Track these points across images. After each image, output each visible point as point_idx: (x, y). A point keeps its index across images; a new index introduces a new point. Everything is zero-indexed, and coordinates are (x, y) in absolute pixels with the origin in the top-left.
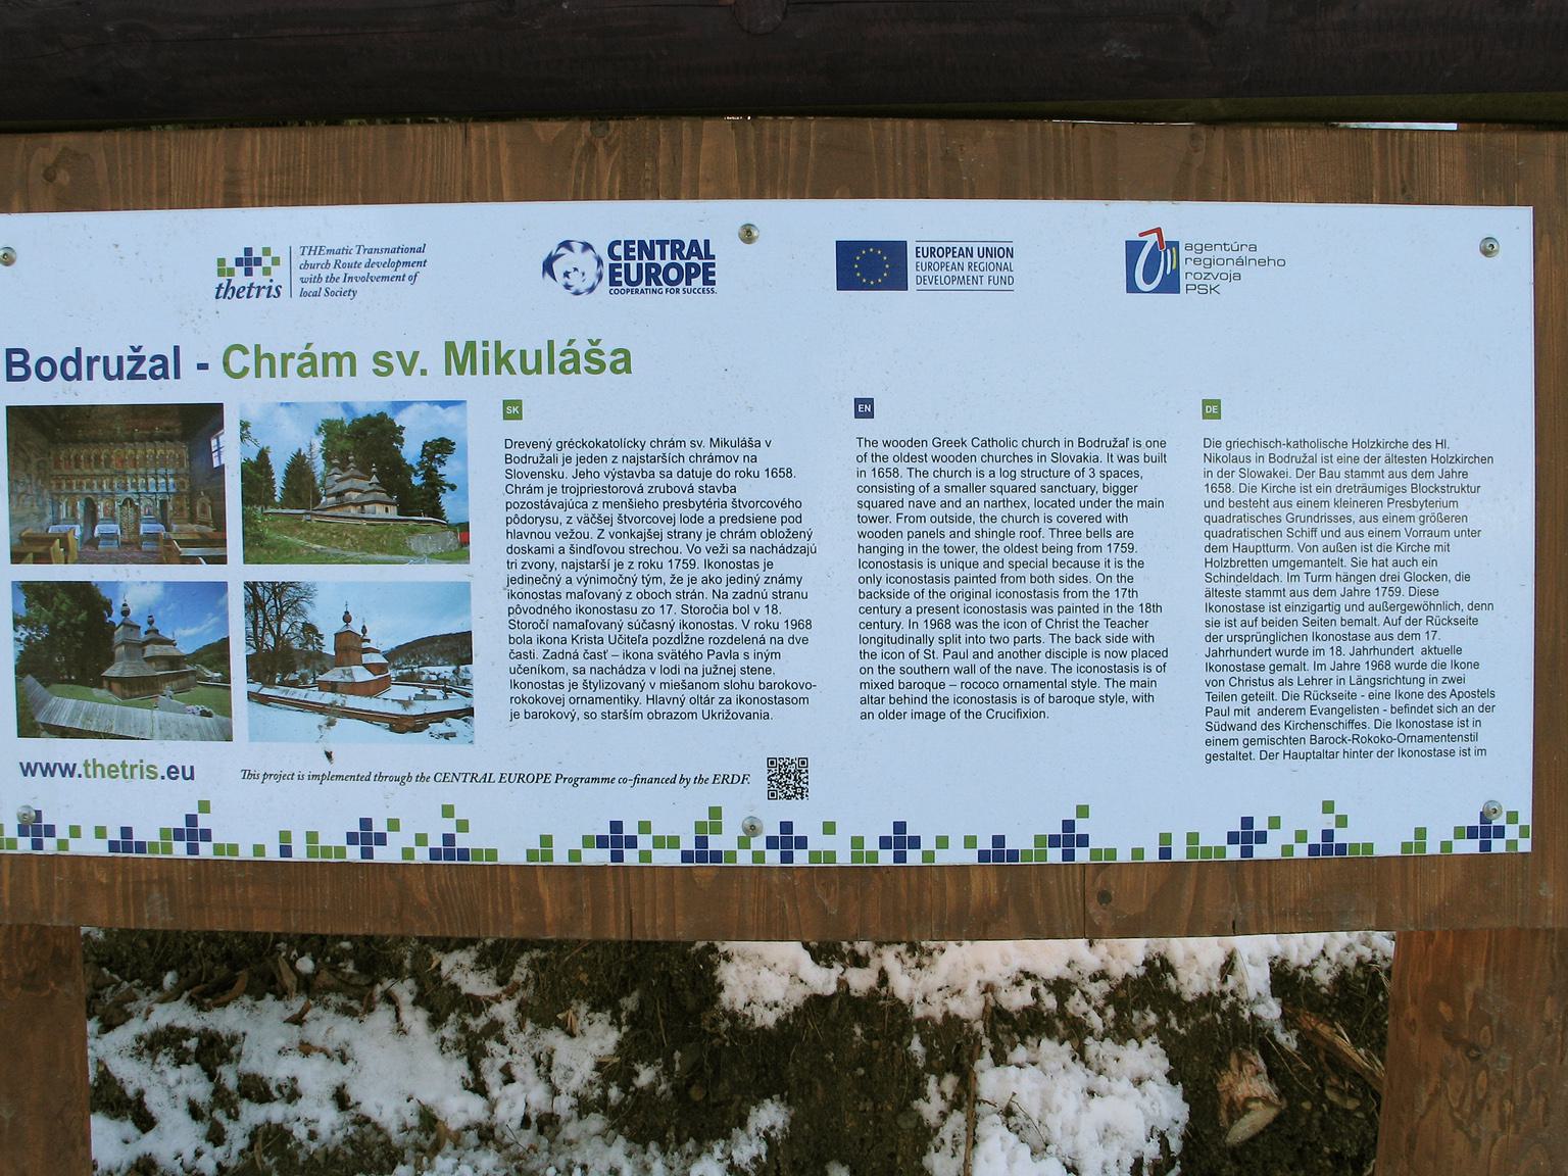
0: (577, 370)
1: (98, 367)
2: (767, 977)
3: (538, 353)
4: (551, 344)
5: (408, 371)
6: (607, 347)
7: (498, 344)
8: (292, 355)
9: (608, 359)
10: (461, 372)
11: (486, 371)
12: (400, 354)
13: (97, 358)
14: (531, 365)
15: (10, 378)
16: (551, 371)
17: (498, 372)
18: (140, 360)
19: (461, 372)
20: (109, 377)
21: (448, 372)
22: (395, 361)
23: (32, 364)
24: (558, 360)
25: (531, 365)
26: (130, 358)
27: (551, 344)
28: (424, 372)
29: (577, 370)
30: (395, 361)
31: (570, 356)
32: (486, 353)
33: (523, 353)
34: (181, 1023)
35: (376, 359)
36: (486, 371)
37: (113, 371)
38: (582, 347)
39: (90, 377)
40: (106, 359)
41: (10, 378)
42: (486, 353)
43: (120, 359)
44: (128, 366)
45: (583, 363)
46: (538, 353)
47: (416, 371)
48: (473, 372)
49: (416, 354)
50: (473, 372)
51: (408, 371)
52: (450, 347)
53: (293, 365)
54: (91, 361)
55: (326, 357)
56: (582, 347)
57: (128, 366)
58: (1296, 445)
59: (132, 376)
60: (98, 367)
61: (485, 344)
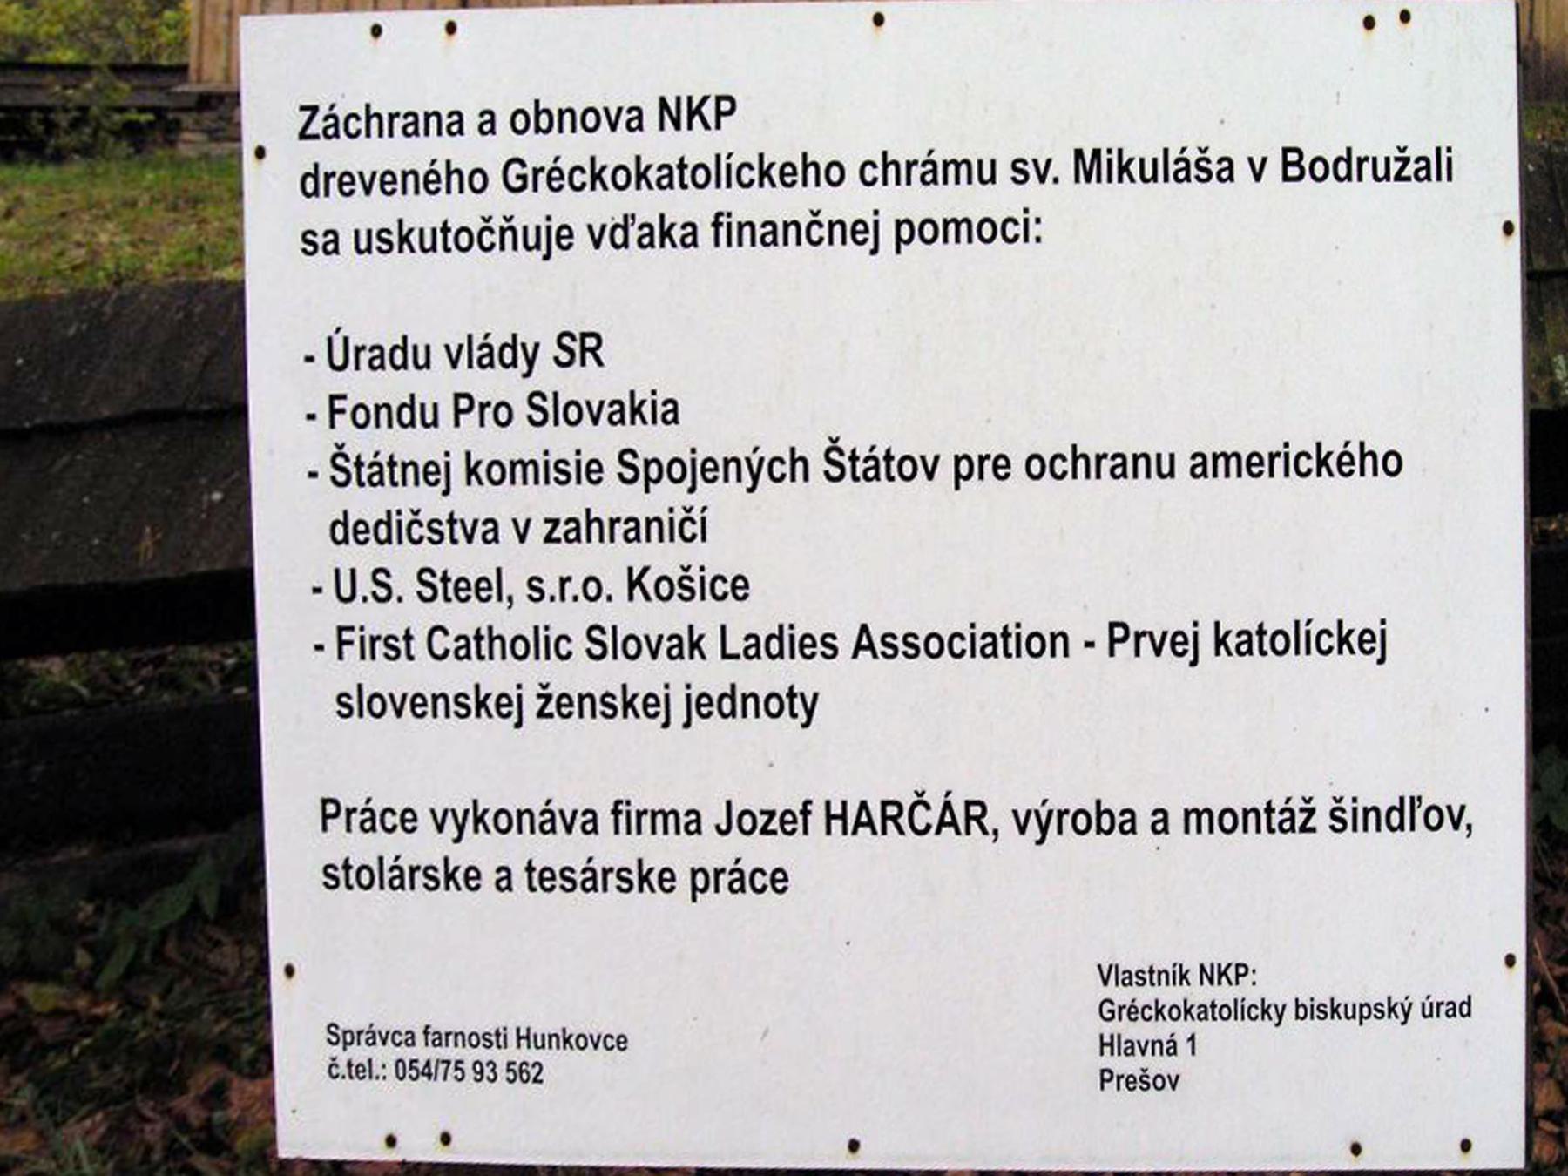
0: (1188, 178)
1: (1367, 167)
2: (171, 116)
3: (1155, 161)
4: (1166, 151)
5: (1042, 179)
6: (1213, 155)
7: (1120, 151)
8: (915, 162)
9: (1214, 168)
10: (1088, 180)
11: (1110, 180)
12: (1035, 162)
13: (1366, 159)
14: (1149, 174)
15: (1286, 178)
16: (1166, 180)
17: (1120, 180)
18: (1406, 161)
19: (1088, 180)
20: (1377, 179)
21: (1077, 180)
22: (1030, 169)
23: (1306, 163)
24: (1172, 168)
25: (1149, 174)
26: (1397, 159)
27: (1166, 151)
28: (1056, 180)
29: (1188, 178)
30: (1030, 169)
31: (1182, 165)
32: (1110, 161)
33: (1142, 161)
34: (74, 135)
35: (1015, 168)
36: (1110, 180)
37: (1381, 173)
38: (1193, 155)
39: (1360, 179)
40: (1375, 159)
41: (1286, 178)
42: (1110, 161)
43: (1387, 160)
44: (1395, 167)
45: (1194, 171)
46: (1155, 161)
47: (1049, 179)
48: (1099, 180)
49: (1049, 162)
50: (1099, 180)
51: (1042, 179)
52: (1079, 154)
53: (917, 172)
54: (1361, 161)
55: (946, 164)
56: (1193, 155)
57: (1395, 167)
58: (380, 358)
59: (1399, 178)
60: (1367, 167)
61: (1109, 151)
